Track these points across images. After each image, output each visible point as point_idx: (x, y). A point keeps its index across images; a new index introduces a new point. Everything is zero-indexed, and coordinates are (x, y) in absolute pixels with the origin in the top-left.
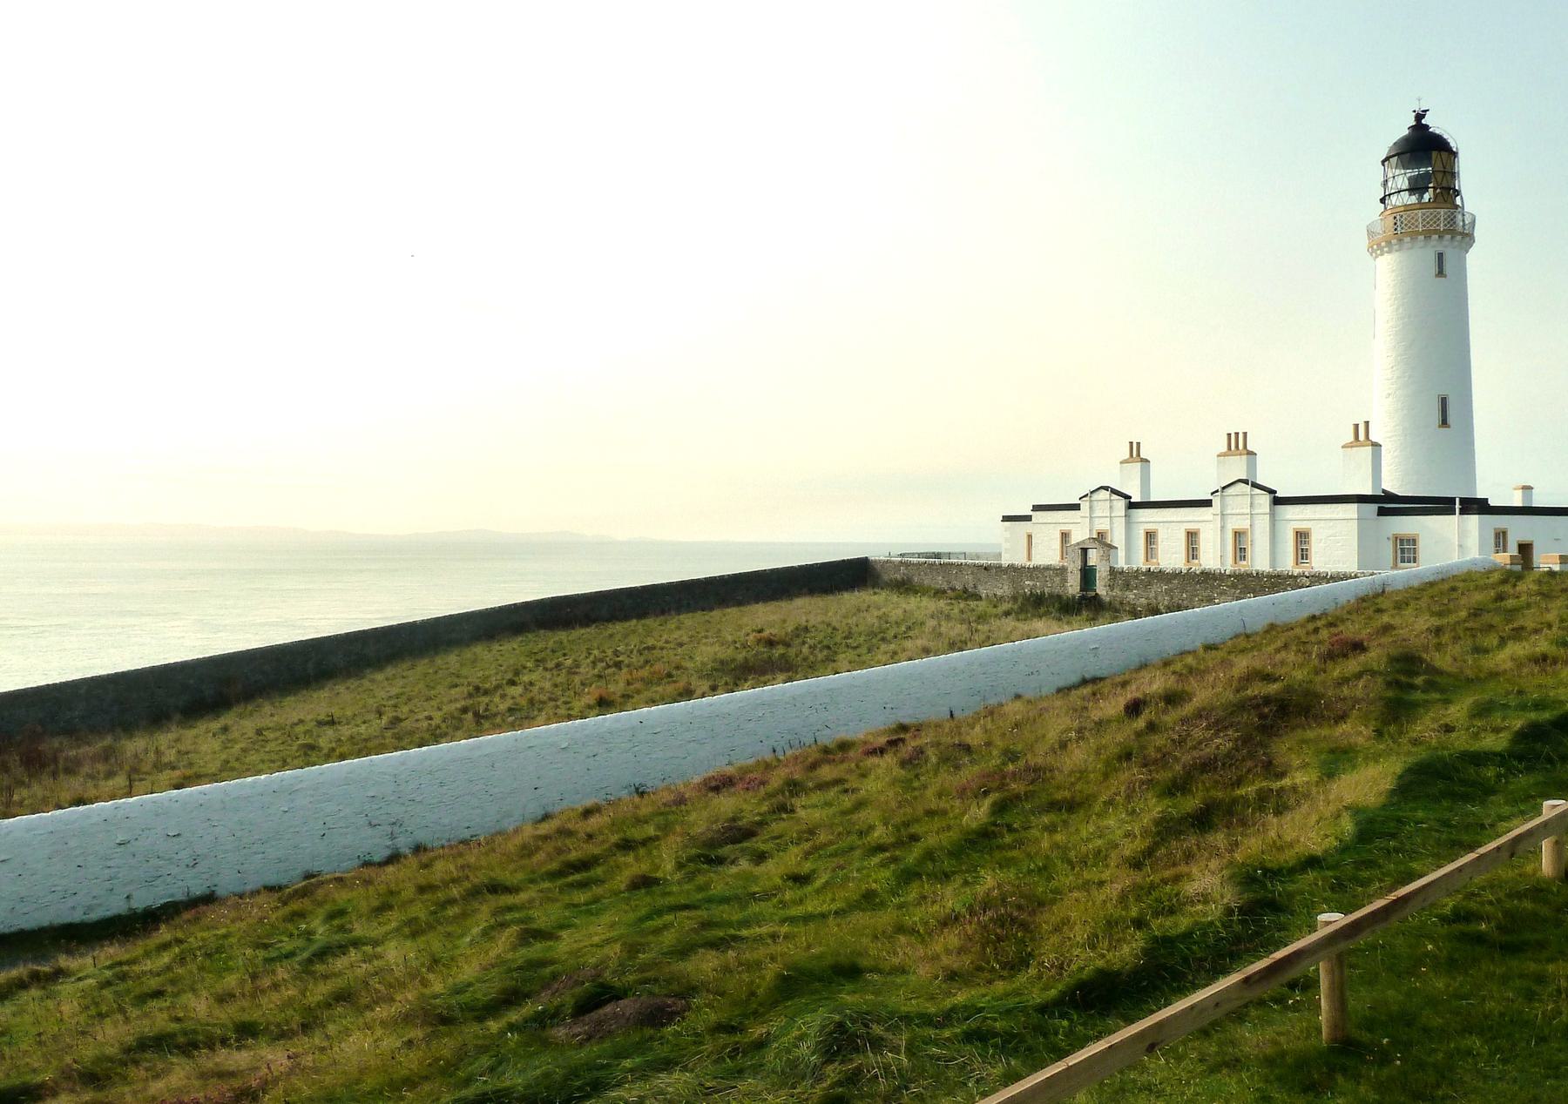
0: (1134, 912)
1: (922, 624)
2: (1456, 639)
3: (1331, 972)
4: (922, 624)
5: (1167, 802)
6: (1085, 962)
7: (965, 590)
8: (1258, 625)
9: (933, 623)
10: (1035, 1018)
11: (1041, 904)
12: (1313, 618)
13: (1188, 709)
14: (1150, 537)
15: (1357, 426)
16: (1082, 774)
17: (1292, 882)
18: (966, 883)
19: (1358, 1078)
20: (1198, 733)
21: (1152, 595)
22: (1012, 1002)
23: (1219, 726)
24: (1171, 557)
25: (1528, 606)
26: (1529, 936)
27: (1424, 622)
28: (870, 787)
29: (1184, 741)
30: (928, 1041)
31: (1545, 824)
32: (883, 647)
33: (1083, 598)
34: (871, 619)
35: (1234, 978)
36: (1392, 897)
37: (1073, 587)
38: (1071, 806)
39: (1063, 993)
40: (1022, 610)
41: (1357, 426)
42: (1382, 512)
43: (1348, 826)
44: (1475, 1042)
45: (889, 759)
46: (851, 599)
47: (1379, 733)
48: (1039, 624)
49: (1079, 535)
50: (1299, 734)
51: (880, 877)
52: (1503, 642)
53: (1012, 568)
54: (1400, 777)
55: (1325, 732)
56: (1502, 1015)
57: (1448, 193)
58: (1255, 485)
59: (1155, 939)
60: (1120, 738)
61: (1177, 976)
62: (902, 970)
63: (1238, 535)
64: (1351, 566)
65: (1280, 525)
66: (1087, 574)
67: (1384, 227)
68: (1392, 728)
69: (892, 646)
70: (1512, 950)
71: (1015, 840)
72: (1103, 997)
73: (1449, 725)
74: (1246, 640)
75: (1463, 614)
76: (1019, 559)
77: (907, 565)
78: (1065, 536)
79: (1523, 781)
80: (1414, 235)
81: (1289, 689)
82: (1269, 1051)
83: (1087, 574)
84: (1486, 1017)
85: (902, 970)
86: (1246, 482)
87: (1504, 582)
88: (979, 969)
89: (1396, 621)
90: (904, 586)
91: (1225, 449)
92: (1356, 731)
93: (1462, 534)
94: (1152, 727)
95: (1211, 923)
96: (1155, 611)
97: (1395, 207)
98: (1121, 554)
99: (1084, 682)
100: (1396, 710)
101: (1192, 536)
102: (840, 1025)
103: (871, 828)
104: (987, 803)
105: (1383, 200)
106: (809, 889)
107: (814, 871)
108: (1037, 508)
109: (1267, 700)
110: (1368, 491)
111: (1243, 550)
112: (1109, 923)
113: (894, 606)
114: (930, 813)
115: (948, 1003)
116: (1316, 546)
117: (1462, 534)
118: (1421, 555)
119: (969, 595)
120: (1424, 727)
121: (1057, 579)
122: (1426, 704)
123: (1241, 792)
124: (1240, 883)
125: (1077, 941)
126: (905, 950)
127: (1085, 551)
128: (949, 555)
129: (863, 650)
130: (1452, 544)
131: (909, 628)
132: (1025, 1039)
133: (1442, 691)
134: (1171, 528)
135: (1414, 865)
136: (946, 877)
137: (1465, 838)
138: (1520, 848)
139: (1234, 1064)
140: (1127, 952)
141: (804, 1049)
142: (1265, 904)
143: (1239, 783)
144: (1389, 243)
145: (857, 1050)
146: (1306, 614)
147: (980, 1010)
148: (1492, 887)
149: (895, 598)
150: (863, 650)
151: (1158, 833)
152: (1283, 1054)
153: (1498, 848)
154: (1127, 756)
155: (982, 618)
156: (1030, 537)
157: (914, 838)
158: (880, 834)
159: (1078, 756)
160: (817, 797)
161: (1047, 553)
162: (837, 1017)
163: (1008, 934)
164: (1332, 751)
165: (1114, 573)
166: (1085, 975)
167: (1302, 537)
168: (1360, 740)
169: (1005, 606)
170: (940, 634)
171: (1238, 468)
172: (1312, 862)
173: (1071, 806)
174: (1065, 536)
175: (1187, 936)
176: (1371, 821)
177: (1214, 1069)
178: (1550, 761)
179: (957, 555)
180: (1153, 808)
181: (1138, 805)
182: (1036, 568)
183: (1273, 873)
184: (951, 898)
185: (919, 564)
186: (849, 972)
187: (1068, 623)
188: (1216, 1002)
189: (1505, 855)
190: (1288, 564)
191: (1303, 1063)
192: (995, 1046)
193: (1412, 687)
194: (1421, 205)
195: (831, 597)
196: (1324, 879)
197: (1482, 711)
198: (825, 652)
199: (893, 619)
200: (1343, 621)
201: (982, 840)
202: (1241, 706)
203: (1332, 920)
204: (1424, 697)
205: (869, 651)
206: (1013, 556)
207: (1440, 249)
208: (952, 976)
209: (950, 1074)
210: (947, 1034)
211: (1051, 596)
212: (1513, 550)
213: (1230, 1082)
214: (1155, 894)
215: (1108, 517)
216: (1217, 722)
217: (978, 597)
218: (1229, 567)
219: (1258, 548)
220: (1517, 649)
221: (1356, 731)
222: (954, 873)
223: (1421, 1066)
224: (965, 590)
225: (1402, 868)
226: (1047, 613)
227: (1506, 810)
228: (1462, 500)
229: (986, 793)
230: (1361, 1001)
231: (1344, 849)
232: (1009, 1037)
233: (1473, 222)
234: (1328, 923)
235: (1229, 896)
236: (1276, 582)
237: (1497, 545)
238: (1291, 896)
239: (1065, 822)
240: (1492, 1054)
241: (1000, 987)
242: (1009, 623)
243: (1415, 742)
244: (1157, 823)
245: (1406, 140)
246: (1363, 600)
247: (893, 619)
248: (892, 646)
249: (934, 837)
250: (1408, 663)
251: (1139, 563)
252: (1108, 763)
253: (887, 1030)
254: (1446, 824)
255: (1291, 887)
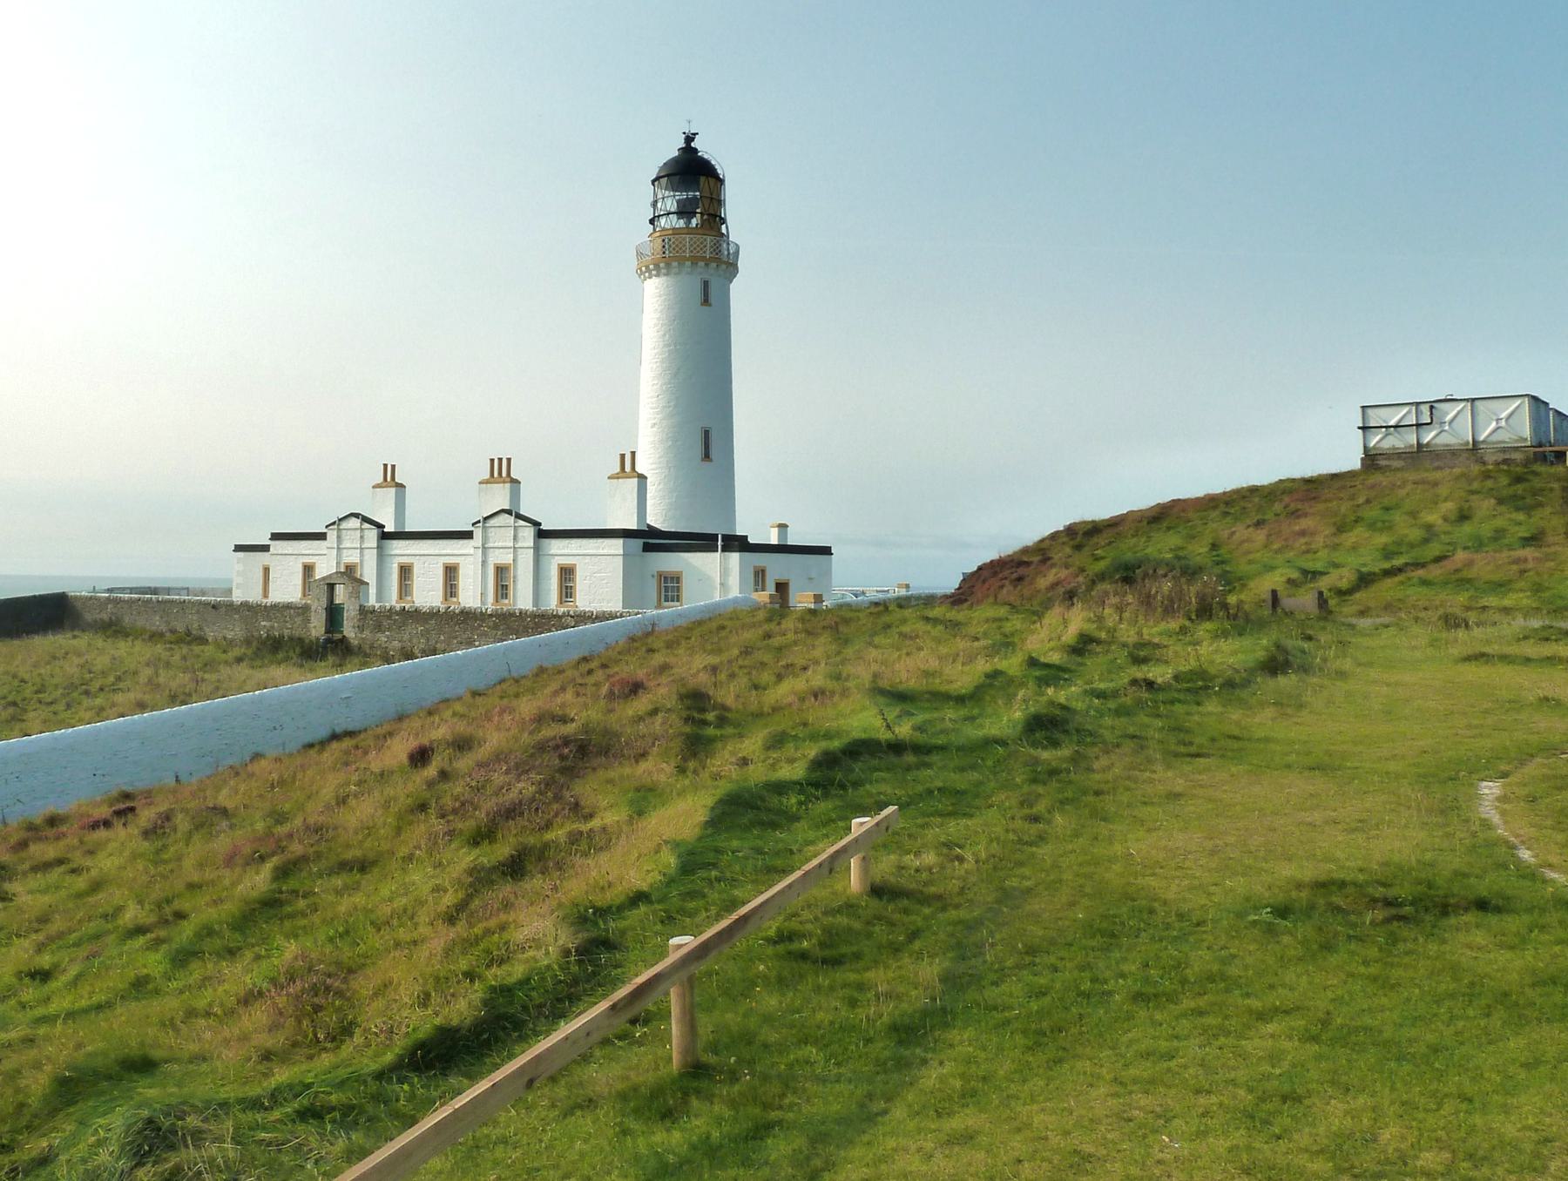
0: (463, 964)
1: (135, 673)
2: (732, 676)
3: (682, 996)
4: (135, 673)
5: (477, 851)
6: (420, 1023)
7: (188, 633)
8: (526, 668)
9: (148, 671)
10: (373, 1087)
11: (351, 971)
12: (585, 659)
13: (482, 753)
14: (405, 571)
15: (623, 456)
16: (369, 830)
17: (624, 919)
18: (258, 958)
19: (710, 1098)
20: (498, 778)
21: (406, 637)
22: (342, 1073)
23: (521, 769)
24: (427, 594)
25: (795, 643)
26: (845, 949)
27: (701, 661)
28: (105, 863)
29: (484, 787)
30: (256, 1127)
31: (856, 840)
32: (86, 702)
33: (328, 641)
34: (71, 668)
35: (603, 1006)
36: (734, 916)
37: (317, 628)
38: (363, 866)
39: (401, 1058)
40: (257, 654)
41: (623, 456)
42: (647, 548)
43: (670, 860)
44: (811, 1051)
45: (120, 832)
46: (43, 643)
47: (682, 770)
48: (277, 672)
49: (325, 568)
50: (601, 773)
51: (154, 963)
52: (780, 678)
53: (246, 605)
54: (713, 809)
55: (627, 771)
56: (832, 1023)
57: (714, 220)
58: (519, 516)
59: (493, 989)
60: (411, 788)
61: (518, 1025)
62: (202, 1058)
63: (501, 571)
64: (614, 604)
65: (544, 560)
66: (334, 614)
67: (653, 248)
68: (692, 765)
69: (98, 701)
70: (836, 962)
71: (308, 906)
72: (444, 1055)
73: (744, 759)
74: (512, 685)
75: (736, 652)
76: (254, 596)
77: (117, 601)
78: (308, 570)
79: (822, 807)
80: (681, 260)
81: (586, 729)
82: (620, 1086)
83: (334, 614)
84: (819, 1027)
85: (202, 1058)
86: (509, 512)
87: (769, 620)
88: (295, 1044)
89: (671, 660)
90: (112, 628)
91: (487, 476)
92: (657, 769)
93: (725, 572)
94: (444, 775)
95: (548, 967)
96: (409, 656)
97: (664, 229)
98: (372, 591)
99: (335, 737)
100: (696, 746)
101: (451, 572)
102: (150, 1121)
103: (120, 909)
104: (268, 866)
105: (652, 221)
106: (54, 985)
107: (56, 966)
108: (276, 537)
109: (566, 741)
110: (632, 525)
111: (505, 587)
112: (437, 979)
113: (99, 652)
114: (192, 887)
115: (273, 1082)
116: (581, 583)
117: (725, 572)
118: (685, 593)
119: (193, 638)
120: (723, 761)
121: (298, 620)
122: (723, 738)
123: (549, 836)
124: (573, 924)
125: (405, 1000)
126: (206, 1034)
127: (331, 587)
128: (168, 591)
129: (60, 707)
130: (715, 580)
131: (119, 679)
132: (359, 1111)
133: (737, 725)
134: (427, 561)
135: (736, 892)
136: (231, 953)
137: (779, 862)
138: (833, 865)
139: (590, 1103)
140: (463, 1008)
141: (104, 1157)
142: (596, 949)
143: (548, 826)
144: (657, 267)
145: (172, 1147)
146: (576, 656)
147: (309, 1086)
148: (809, 906)
149: (100, 643)
150: (60, 707)
151: (471, 885)
152: (635, 1089)
153: (820, 865)
154: (423, 807)
155: (209, 665)
156: (266, 570)
157: (180, 916)
158: (132, 914)
159: (364, 810)
160: (38, 880)
161: (287, 589)
162: (146, 1113)
163: (322, 1006)
164: (638, 790)
165: (364, 612)
166: (421, 1035)
167: (567, 573)
168: (663, 778)
169: (237, 652)
170: (158, 685)
171: (499, 498)
172: (639, 898)
173: (363, 866)
174: (308, 570)
175: (526, 981)
176: (691, 853)
177: (569, 1112)
178: (843, 787)
179: (178, 590)
180: (465, 859)
181: (447, 855)
182: (275, 607)
183: (603, 912)
184: (239, 975)
185: (131, 602)
186: (143, 1066)
187: (311, 670)
188: (587, 1031)
189: (825, 871)
190: (552, 602)
191: (657, 1092)
192: (333, 1121)
193: (705, 723)
194: (688, 230)
195: (16, 642)
196: (654, 912)
197: (777, 741)
198: (11, 710)
199: (98, 667)
200: (617, 662)
201: (271, 904)
202: (541, 747)
203: (683, 942)
204: (718, 733)
205: (68, 706)
206: (246, 591)
207: (706, 277)
208: (267, 1056)
209: (285, 1159)
210: (276, 1114)
211: (291, 639)
212: (771, 589)
213: (584, 1123)
214: (482, 946)
215: (359, 549)
216: (517, 766)
217: (202, 640)
218: (490, 606)
219: (520, 586)
220: (797, 684)
221: (657, 769)
222: (240, 949)
223: (765, 1078)
224: (188, 633)
225: (725, 896)
226: (287, 659)
227: (811, 835)
228: (725, 537)
229: (262, 859)
230: (706, 1025)
231: (671, 882)
232: (347, 1109)
233: (737, 252)
234: (680, 946)
235: (567, 938)
236: (540, 621)
237: (756, 583)
238: (623, 933)
239: (358, 883)
240: (827, 1061)
241: (326, 1060)
242: (243, 671)
243: (716, 777)
244: (471, 872)
245: (675, 161)
246: (633, 639)
247: (98, 667)
248: (98, 701)
249: (203, 912)
250: (696, 700)
251: (393, 600)
252: (400, 817)
253: (206, 1120)
254: (759, 851)
255: (622, 924)
